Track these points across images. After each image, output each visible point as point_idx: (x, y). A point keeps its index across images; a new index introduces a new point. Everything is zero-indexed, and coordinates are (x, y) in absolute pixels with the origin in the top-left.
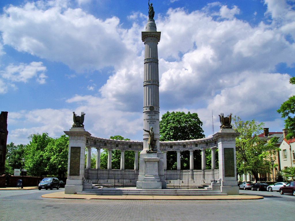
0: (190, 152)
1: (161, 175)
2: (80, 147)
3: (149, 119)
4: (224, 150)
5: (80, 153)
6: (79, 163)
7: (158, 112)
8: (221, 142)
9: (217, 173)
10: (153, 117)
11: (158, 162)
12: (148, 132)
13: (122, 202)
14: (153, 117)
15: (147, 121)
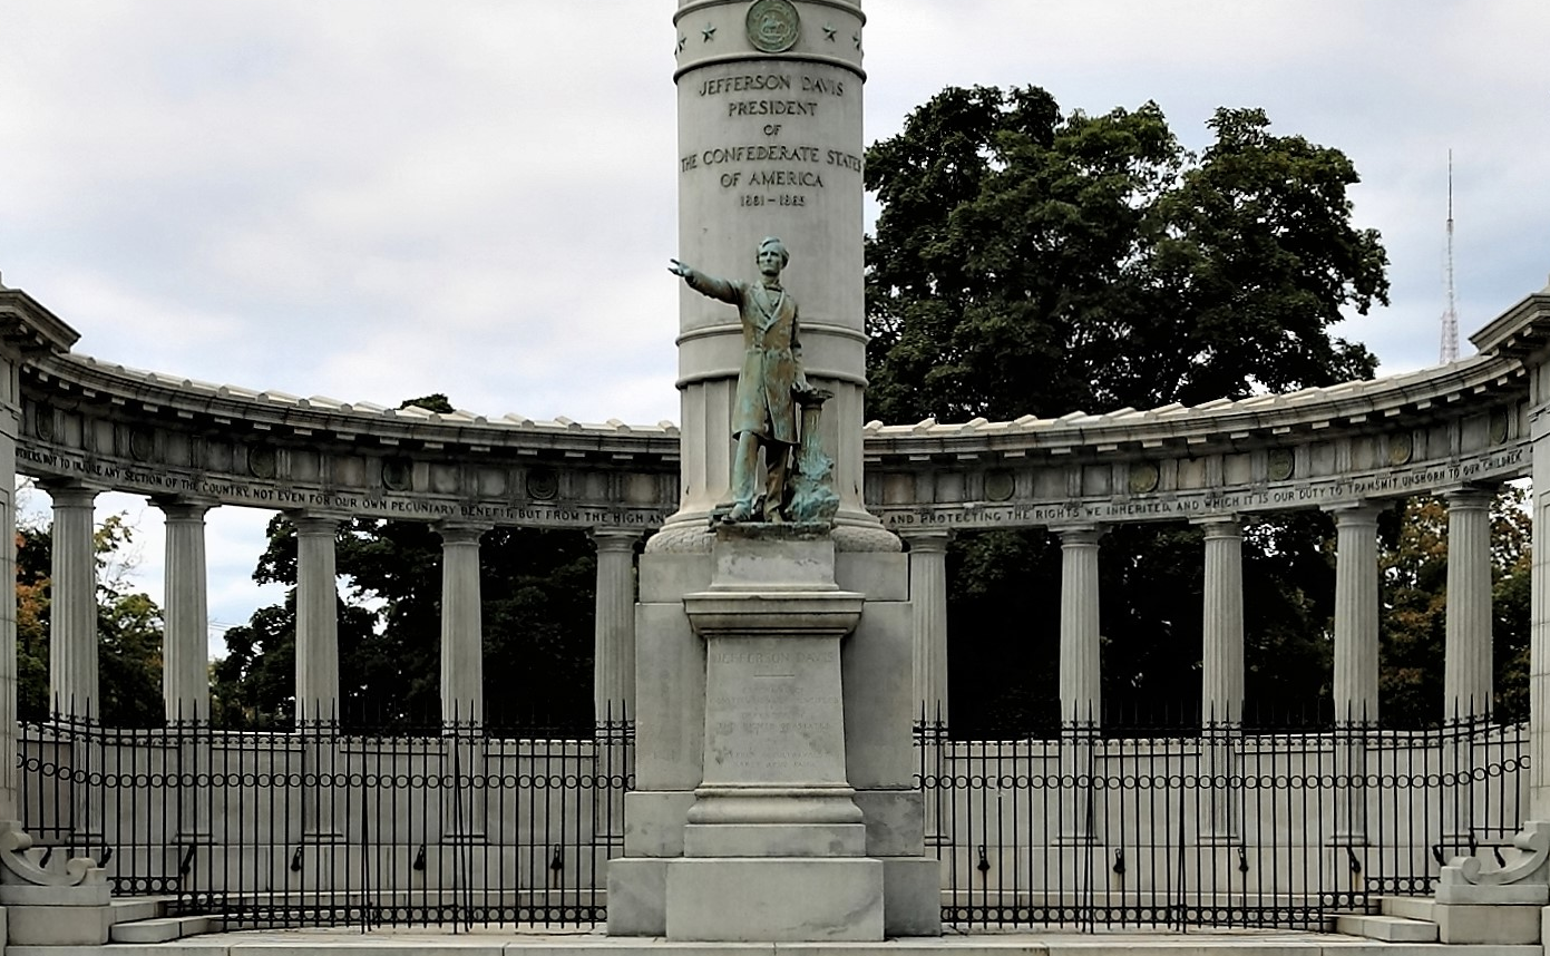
0: (1057, 540)
1: (883, 784)
3: (736, 154)
9: (1510, 766)
10: (794, 132)
11: (847, 641)
12: (734, 296)
14: (794, 132)
15: (716, 171)
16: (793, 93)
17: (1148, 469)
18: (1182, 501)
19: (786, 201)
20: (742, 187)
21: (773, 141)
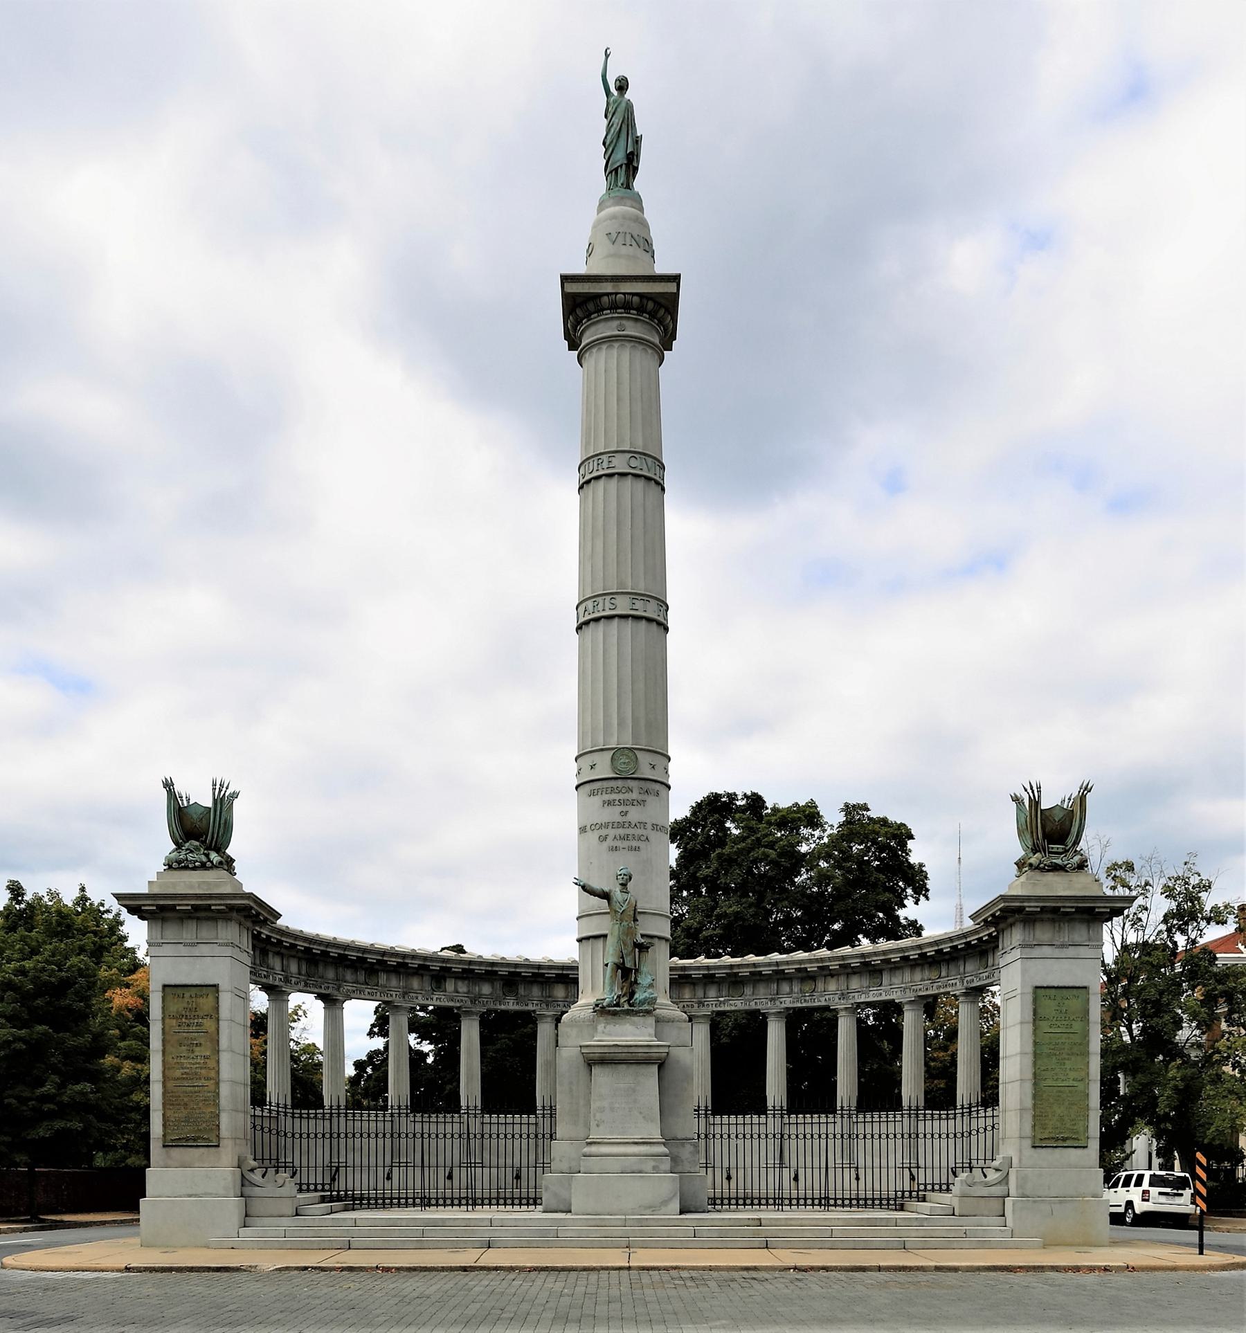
2: (216, 986)
3: (606, 826)
4: (1035, 1000)
5: (218, 1020)
6: (213, 1074)
7: (662, 783)
8: (1017, 953)
9: (989, 1128)
10: (635, 814)
11: (661, 1066)
12: (605, 896)
13: (451, 1284)
14: (635, 814)
16: (635, 795)
17: (810, 982)
18: (827, 997)
19: (631, 849)
20: (609, 842)
21: (624, 819)
